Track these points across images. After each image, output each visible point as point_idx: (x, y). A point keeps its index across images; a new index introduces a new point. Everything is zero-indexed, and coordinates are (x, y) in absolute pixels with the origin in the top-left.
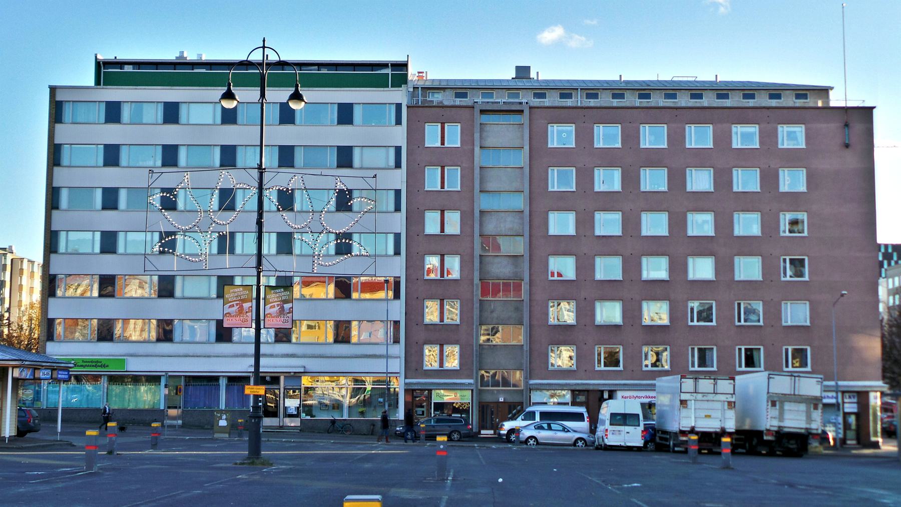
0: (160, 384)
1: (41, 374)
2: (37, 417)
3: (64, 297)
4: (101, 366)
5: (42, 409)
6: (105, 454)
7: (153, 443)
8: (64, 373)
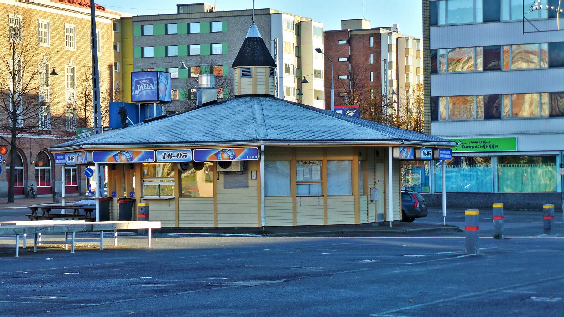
0: (556, 165)
1: (422, 154)
2: (423, 201)
3: (447, 73)
4: (490, 147)
5: (431, 194)
6: (492, 238)
7: (546, 228)
8: (446, 152)
